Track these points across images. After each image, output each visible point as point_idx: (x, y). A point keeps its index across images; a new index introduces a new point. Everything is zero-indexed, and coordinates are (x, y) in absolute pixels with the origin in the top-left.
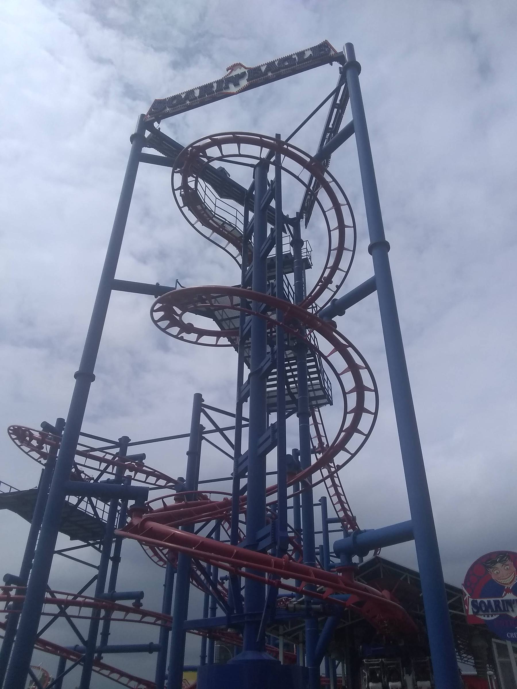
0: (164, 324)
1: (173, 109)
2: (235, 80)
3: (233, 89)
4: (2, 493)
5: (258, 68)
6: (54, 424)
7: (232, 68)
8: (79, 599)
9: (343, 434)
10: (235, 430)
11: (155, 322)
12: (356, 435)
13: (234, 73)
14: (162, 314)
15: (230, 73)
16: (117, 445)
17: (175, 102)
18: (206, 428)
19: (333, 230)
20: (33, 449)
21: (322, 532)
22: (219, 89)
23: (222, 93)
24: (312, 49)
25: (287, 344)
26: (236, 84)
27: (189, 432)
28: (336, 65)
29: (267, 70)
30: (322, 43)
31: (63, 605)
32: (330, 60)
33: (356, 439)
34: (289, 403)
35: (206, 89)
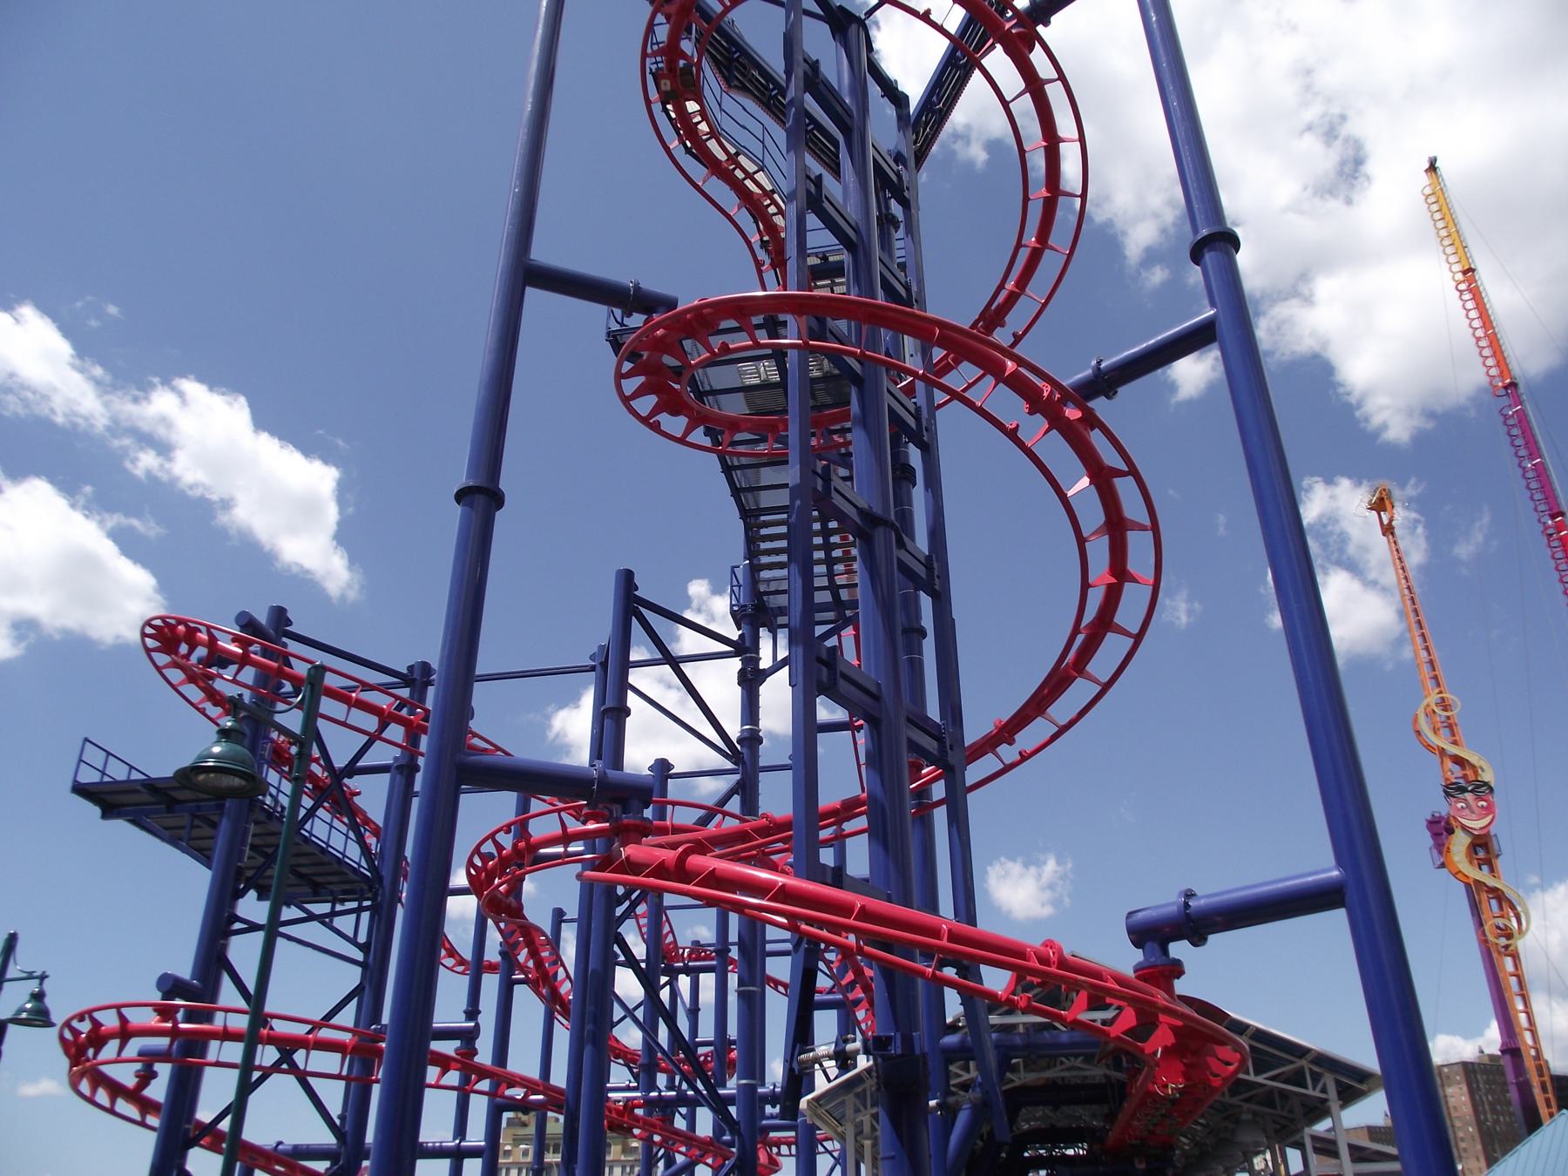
0: (646, 404)
4: (111, 780)
6: (262, 617)
8: (325, 1033)
9: (1080, 638)
11: (626, 400)
12: (1111, 638)
14: (639, 380)
16: (406, 679)
18: (589, 656)
20: (192, 678)
21: (800, 938)
31: (288, 1046)
33: (1112, 648)
34: (824, 607)
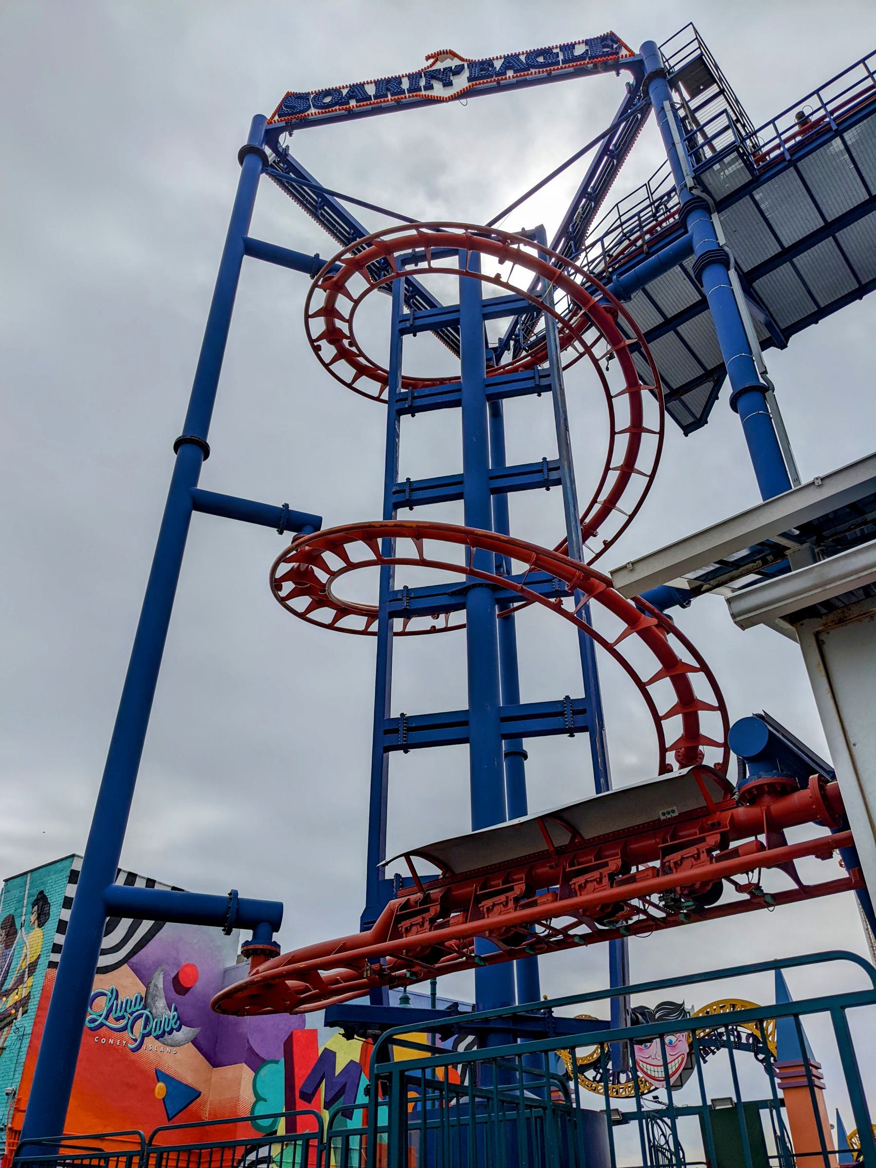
1: (322, 113)
2: (445, 77)
3: (438, 90)
5: (489, 63)
7: (437, 57)
10: (466, 629)
13: (440, 66)
15: (431, 65)
17: (328, 100)
19: (616, 396)
22: (415, 88)
23: (419, 96)
24: (587, 42)
25: (702, 88)
26: (448, 84)
27: (575, 281)
28: (627, 76)
29: (351, 96)
30: (604, 34)
32: (617, 67)
35: (387, 86)
